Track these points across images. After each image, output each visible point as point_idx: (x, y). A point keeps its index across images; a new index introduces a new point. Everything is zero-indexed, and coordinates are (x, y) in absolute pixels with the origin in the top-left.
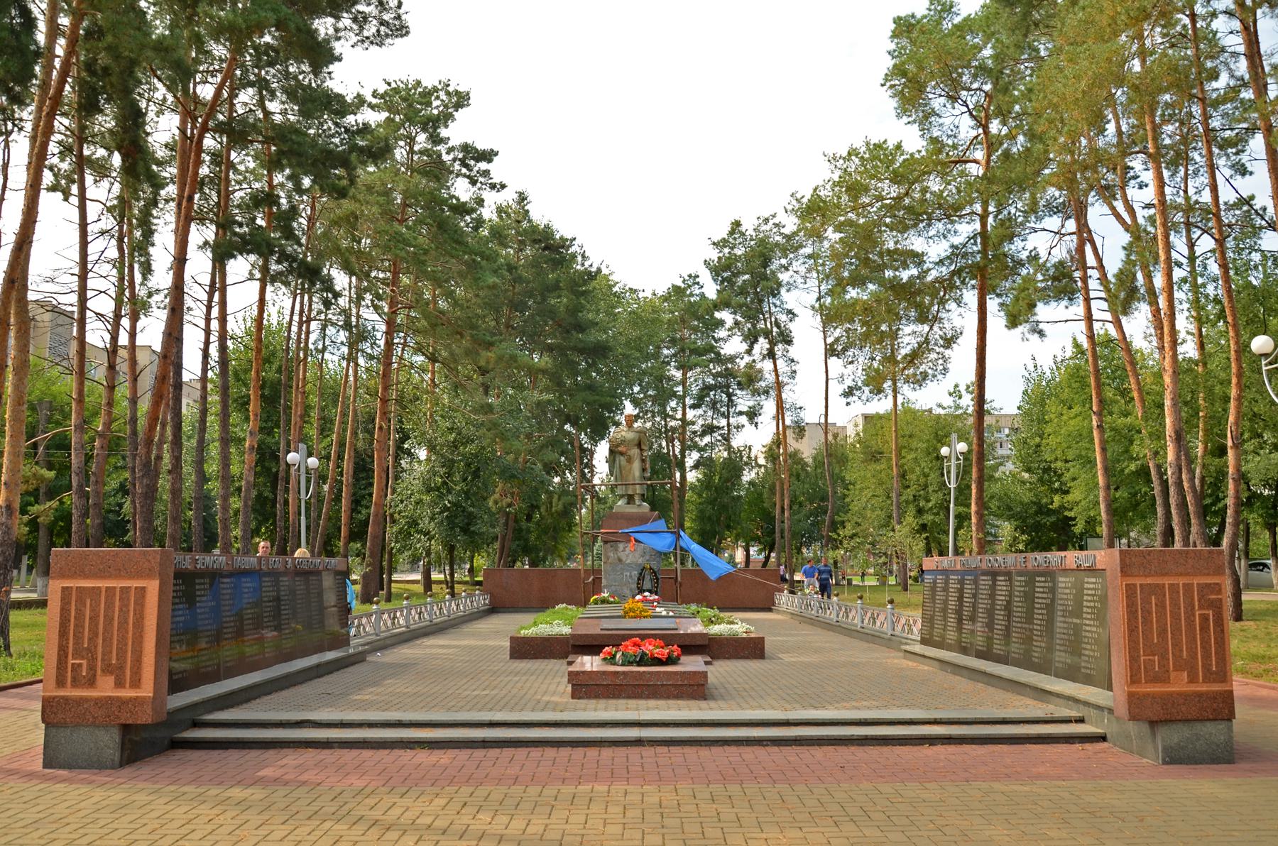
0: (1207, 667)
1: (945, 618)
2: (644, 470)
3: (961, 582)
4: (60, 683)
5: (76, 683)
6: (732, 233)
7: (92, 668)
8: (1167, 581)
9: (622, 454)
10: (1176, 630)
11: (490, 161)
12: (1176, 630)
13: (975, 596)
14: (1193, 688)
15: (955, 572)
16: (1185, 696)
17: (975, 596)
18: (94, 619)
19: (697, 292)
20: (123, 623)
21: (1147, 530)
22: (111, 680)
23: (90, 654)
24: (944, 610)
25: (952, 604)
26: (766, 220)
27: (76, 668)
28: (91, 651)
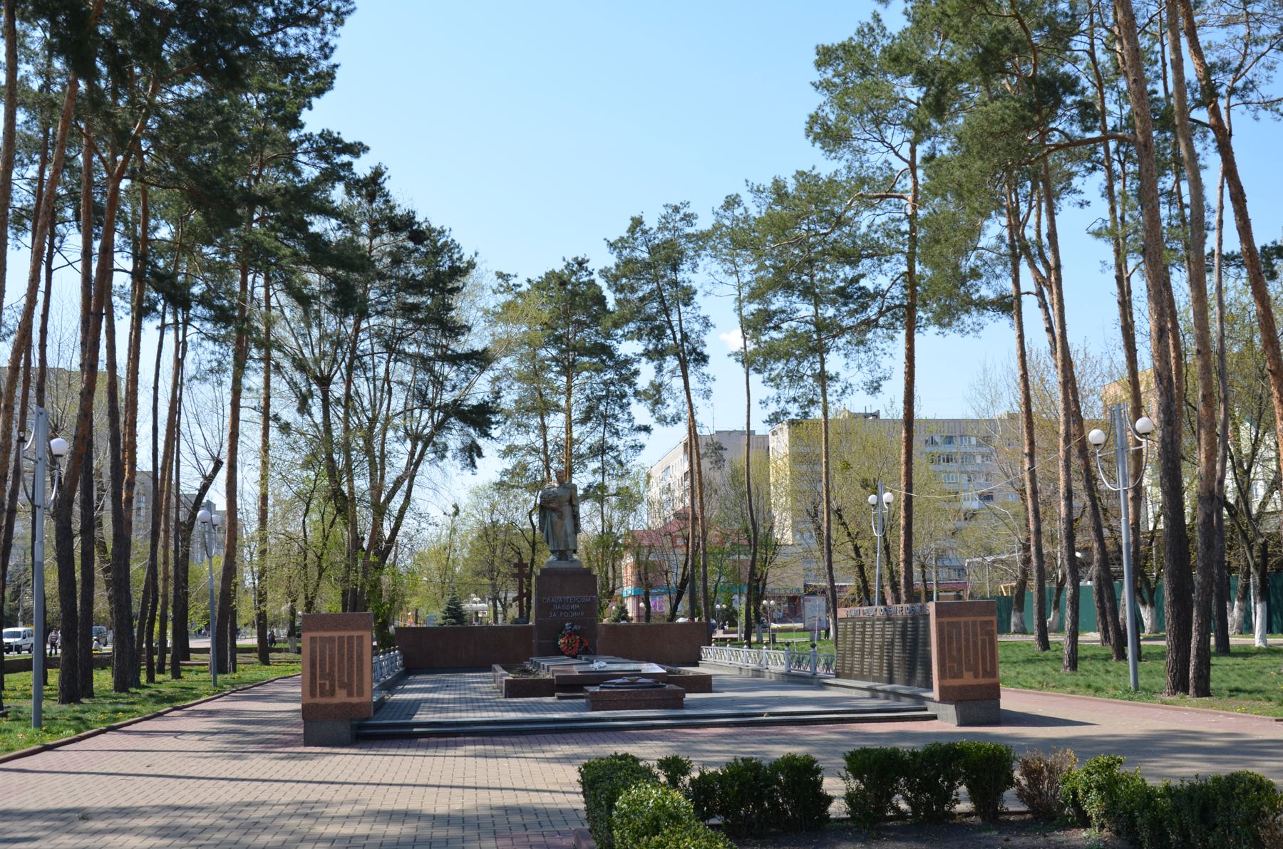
0: (984, 670)
1: (853, 655)
3: (864, 626)
4: (313, 695)
5: (322, 694)
6: (632, 230)
7: (332, 686)
8: (963, 619)
9: (554, 510)
10: (967, 648)
11: (357, 155)
12: (967, 648)
13: (872, 636)
14: (974, 682)
15: (860, 619)
16: (972, 687)
17: (872, 636)
19: (585, 279)
20: (350, 658)
24: (852, 649)
25: (858, 644)
26: (676, 209)
27: (322, 686)
28: (331, 675)
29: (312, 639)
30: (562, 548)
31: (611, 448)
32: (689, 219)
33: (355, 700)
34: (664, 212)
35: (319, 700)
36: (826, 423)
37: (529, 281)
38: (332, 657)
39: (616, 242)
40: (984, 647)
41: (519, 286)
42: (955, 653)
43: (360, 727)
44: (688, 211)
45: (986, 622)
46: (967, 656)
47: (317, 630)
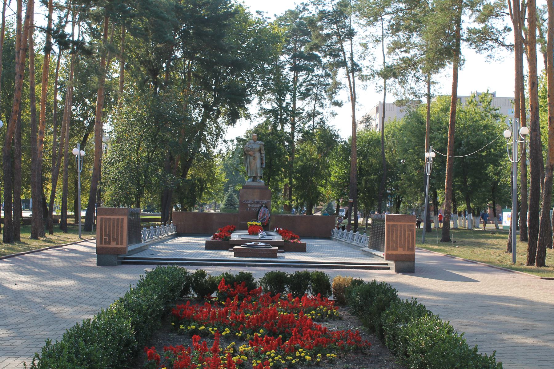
0: (408, 247)
2: (262, 164)
4: (101, 243)
5: (105, 243)
7: (110, 239)
8: (399, 223)
9: (250, 155)
10: (401, 236)
12: (401, 236)
16: (402, 255)
18: (110, 226)
21: (264, 214)
22: (115, 243)
23: (109, 235)
27: (105, 239)
28: (109, 235)
29: (101, 218)
30: (254, 175)
31: (319, 113)
33: (119, 246)
35: (103, 246)
36: (429, 106)
37: (275, 15)
40: (409, 237)
41: (269, 18)
42: (394, 239)
45: (410, 225)
46: (400, 240)
47: (103, 215)
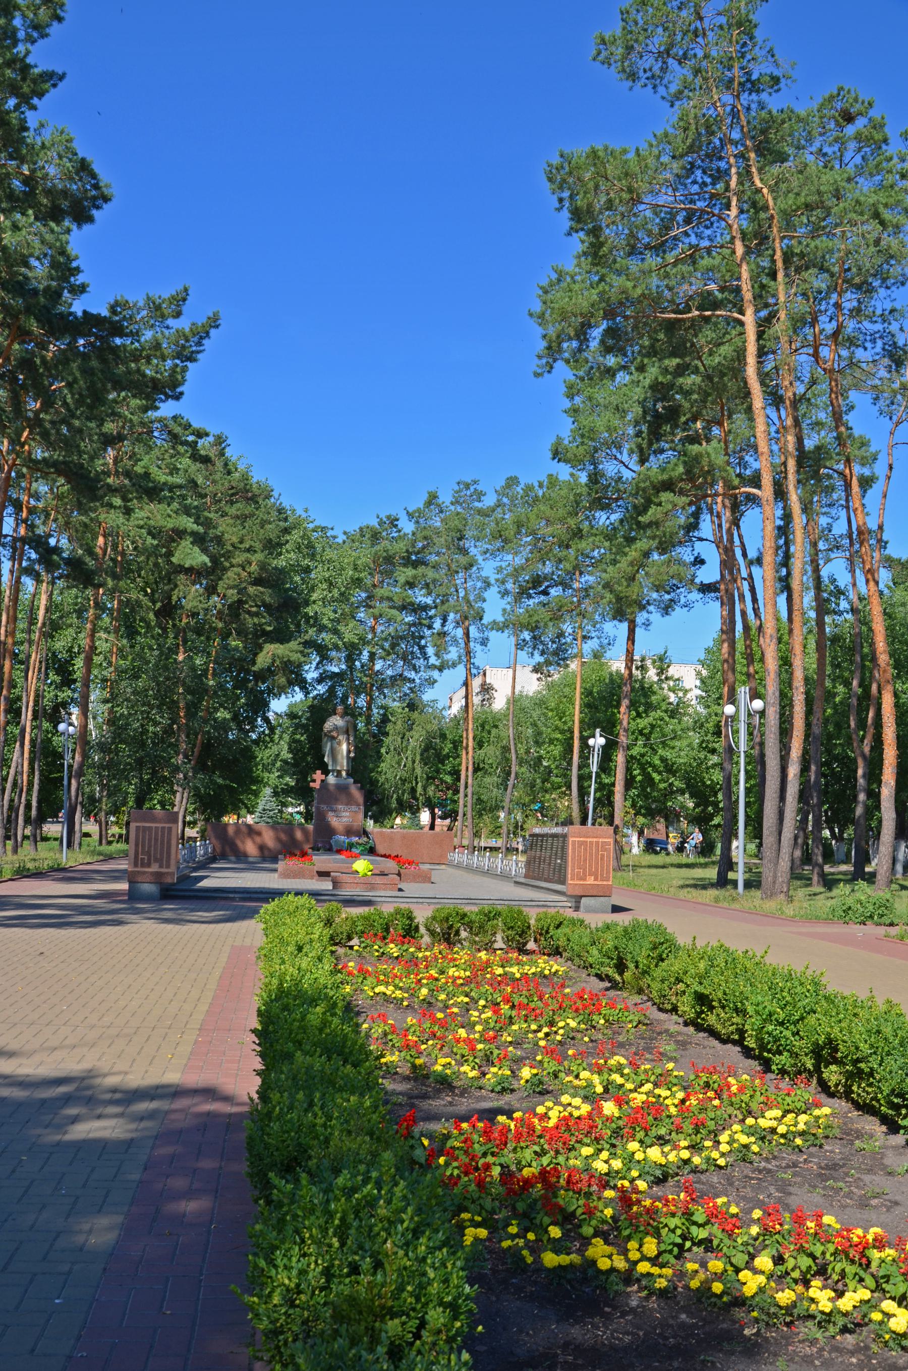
0: (602, 875)
5: (143, 866)
6: (429, 503)
7: (149, 859)
10: (591, 859)
26: (467, 486)
27: (142, 859)
32: (480, 495)
33: (164, 870)
34: (457, 488)
38: (143, 842)
39: (415, 512)
43: (167, 890)
44: (479, 488)
